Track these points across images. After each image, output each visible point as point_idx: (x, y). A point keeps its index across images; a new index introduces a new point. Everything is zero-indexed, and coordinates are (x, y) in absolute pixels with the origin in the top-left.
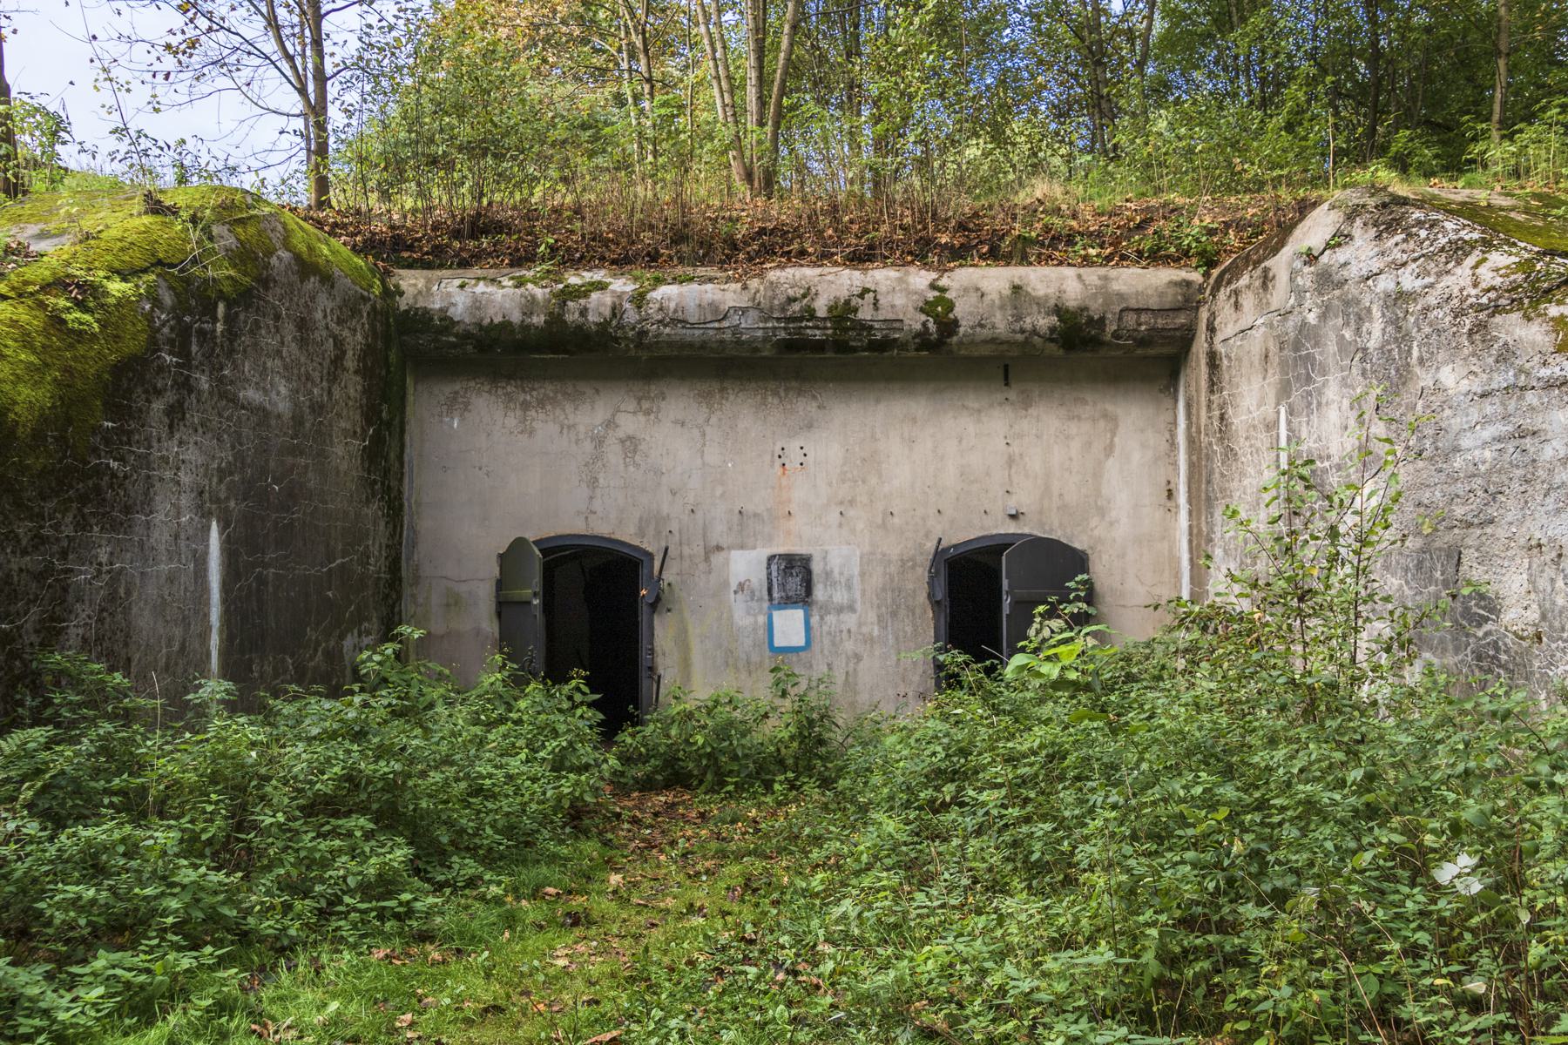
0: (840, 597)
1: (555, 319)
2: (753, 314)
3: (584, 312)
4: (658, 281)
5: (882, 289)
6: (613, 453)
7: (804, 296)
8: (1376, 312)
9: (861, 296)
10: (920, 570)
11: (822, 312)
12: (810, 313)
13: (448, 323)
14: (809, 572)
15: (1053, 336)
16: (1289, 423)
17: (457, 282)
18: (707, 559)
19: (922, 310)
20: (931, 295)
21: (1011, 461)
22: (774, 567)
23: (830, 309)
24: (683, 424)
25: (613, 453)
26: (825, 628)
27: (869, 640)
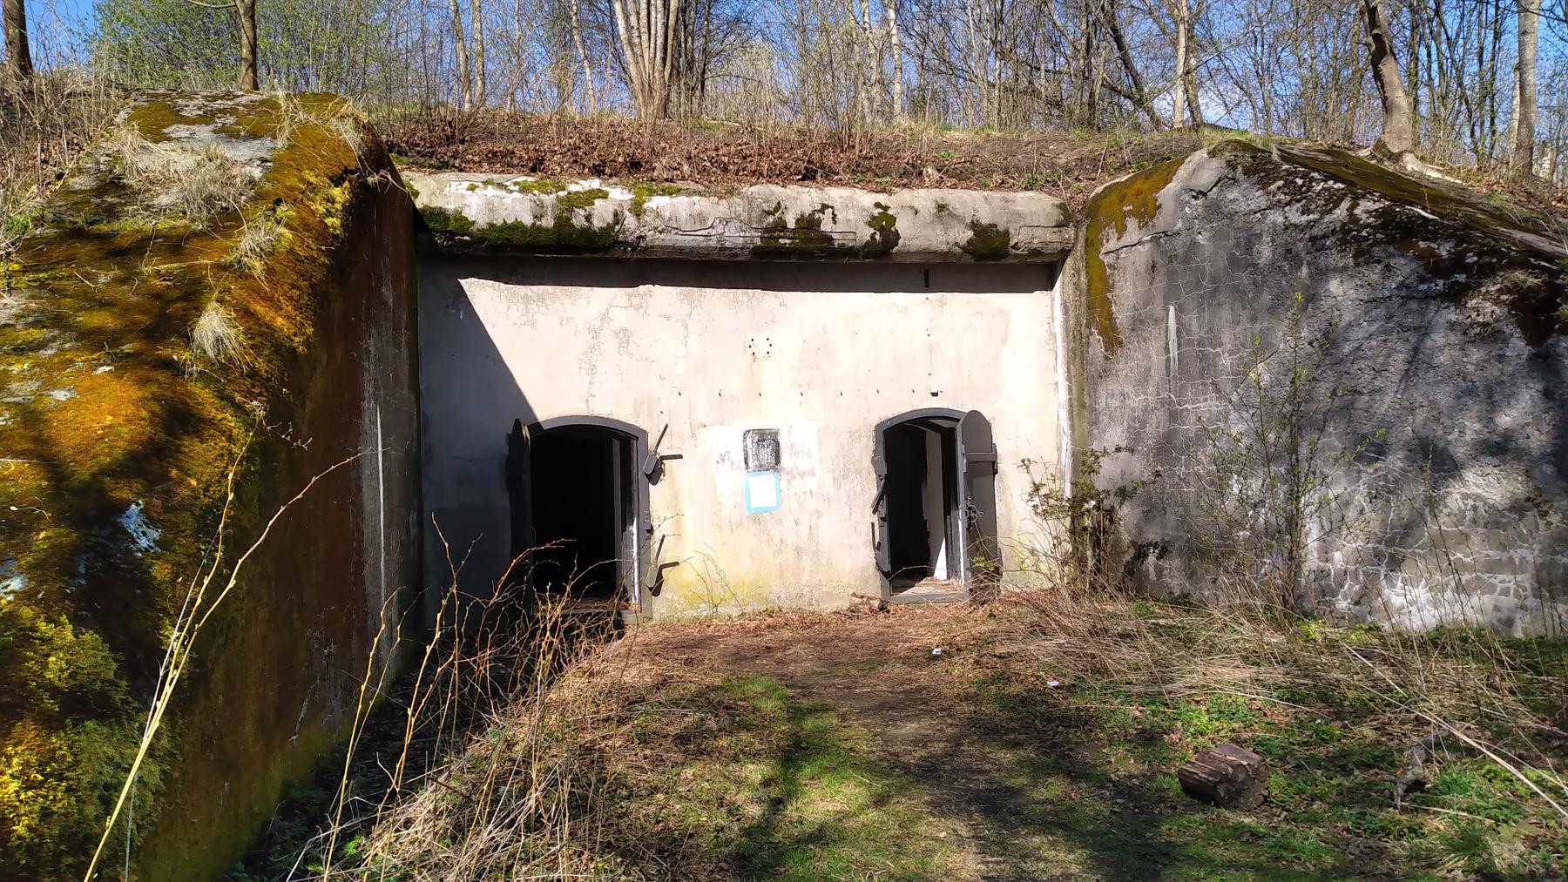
0: (803, 464)
1: (563, 223)
2: (734, 224)
3: (588, 218)
4: (652, 192)
5: (837, 205)
6: (609, 343)
8: (1266, 239)
9: (822, 211)
10: (864, 440)
11: (791, 225)
12: (781, 226)
13: (463, 223)
14: (778, 444)
15: (969, 249)
16: (1178, 318)
17: (466, 184)
18: (693, 435)
19: (870, 224)
20: (877, 212)
21: (931, 349)
22: (749, 441)
23: (798, 222)
24: (668, 318)
25: (609, 343)
26: (792, 490)
27: (827, 499)
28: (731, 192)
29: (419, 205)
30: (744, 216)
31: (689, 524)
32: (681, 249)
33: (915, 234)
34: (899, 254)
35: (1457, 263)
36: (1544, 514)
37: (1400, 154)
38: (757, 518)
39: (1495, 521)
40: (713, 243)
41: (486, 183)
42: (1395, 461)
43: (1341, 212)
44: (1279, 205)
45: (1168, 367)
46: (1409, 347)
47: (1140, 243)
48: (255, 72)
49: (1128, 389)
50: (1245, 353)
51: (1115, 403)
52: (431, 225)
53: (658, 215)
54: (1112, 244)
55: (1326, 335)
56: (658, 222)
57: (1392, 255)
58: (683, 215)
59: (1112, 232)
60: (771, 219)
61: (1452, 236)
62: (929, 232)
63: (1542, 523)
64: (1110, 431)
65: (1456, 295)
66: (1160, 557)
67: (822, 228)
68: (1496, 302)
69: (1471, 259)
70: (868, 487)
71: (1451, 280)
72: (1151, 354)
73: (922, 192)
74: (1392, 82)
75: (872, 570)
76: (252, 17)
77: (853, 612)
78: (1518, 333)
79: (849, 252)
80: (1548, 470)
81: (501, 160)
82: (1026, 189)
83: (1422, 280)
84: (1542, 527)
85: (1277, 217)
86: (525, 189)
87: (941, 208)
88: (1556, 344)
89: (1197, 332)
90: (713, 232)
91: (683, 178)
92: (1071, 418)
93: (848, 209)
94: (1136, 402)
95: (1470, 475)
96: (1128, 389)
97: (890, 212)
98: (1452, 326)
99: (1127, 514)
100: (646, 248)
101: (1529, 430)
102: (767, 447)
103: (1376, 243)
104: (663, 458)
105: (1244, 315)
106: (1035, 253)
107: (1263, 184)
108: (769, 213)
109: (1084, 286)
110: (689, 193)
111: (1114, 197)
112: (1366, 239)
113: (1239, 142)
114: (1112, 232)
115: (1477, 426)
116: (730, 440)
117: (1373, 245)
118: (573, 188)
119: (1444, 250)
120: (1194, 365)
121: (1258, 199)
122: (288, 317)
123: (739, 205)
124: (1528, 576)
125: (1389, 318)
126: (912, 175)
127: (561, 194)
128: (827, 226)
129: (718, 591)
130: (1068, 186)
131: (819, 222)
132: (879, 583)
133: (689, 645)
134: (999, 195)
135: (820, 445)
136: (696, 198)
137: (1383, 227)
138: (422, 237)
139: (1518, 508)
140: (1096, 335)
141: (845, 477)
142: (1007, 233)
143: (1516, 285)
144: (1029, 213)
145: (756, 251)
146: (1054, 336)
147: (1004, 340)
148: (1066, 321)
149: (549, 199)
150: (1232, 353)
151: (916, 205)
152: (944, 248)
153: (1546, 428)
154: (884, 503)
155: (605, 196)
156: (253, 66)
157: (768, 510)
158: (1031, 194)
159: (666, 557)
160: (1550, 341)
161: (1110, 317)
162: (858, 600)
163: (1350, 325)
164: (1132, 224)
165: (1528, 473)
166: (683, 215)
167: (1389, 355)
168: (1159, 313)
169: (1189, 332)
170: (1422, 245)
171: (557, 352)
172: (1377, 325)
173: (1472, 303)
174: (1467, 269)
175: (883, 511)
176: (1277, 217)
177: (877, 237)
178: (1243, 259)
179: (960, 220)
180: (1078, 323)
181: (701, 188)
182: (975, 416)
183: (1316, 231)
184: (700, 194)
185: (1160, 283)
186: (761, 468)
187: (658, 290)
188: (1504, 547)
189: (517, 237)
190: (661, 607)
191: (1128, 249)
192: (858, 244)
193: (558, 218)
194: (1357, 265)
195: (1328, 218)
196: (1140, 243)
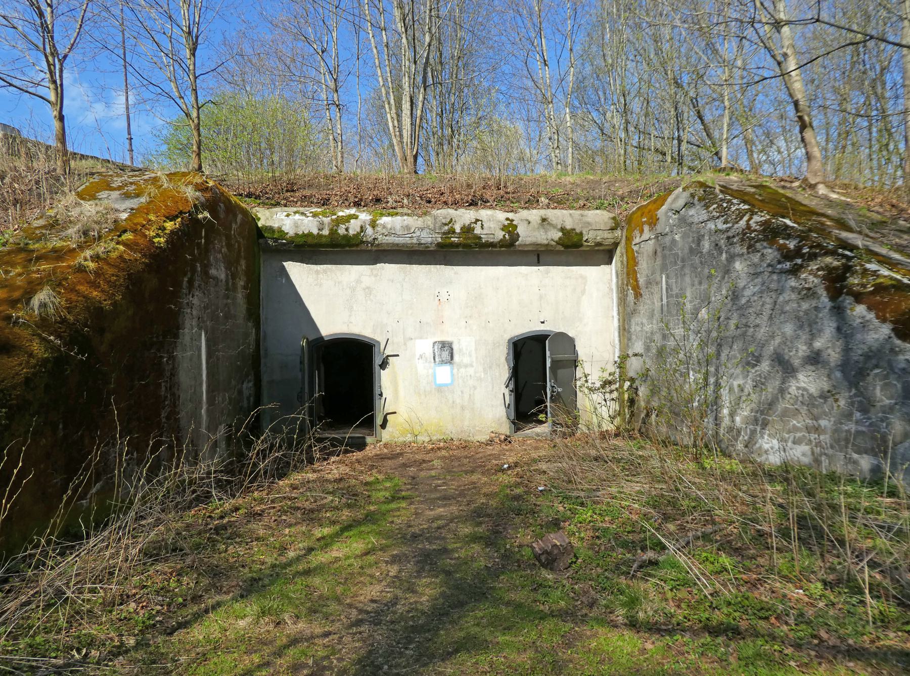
0: (466, 360)
1: (333, 232)
3: (347, 230)
4: (382, 215)
5: (484, 219)
7: (450, 223)
8: (707, 238)
10: (501, 347)
11: (458, 230)
14: (452, 349)
16: (667, 282)
17: (285, 214)
18: (405, 344)
19: (502, 230)
20: (506, 223)
21: (541, 297)
22: (436, 347)
23: (461, 229)
27: (480, 379)
28: (425, 214)
29: (260, 225)
30: (432, 226)
31: (402, 393)
32: (397, 245)
33: (528, 235)
34: (520, 245)
35: (798, 253)
36: (836, 400)
37: (816, 184)
38: (440, 389)
39: (810, 402)
40: (415, 241)
41: (295, 213)
42: (765, 366)
43: (743, 223)
44: (713, 218)
45: (662, 309)
46: (772, 300)
47: (649, 239)
48: (199, 157)
49: (645, 321)
50: (697, 302)
51: (638, 328)
52: (266, 235)
53: (384, 227)
54: (637, 240)
55: (734, 292)
56: (384, 231)
57: (765, 248)
58: (398, 227)
59: (637, 233)
60: (446, 228)
61: (798, 236)
62: (536, 233)
63: (835, 405)
64: (636, 344)
65: (795, 271)
66: (657, 416)
67: (475, 232)
68: (816, 276)
69: (806, 250)
70: (503, 372)
71: (793, 261)
72: (655, 300)
73: (535, 211)
74: (810, 143)
75: (504, 419)
76: (198, 129)
77: (490, 442)
78: (825, 293)
79: (492, 245)
80: (838, 374)
81: (307, 200)
82: (597, 209)
83: (779, 262)
84: (835, 408)
85: (711, 225)
86: (315, 215)
87: (544, 220)
88: (843, 301)
89: (676, 291)
90: (414, 235)
91: (402, 207)
92: (620, 336)
93: (490, 222)
94: (648, 328)
95: (801, 376)
96: (645, 321)
97: (514, 223)
98: (793, 289)
99: (643, 391)
100: (378, 245)
101: (830, 351)
102: (446, 351)
103: (759, 241)
104: (388, 356)
105: (696, 281)
106: (599, 244)
107: (707, 207)
108: (446, 224)
109: (625, 263)
110: (402, 215)
111: (639, 213)
112: (753, 238)
113: (699, 182)
114: (637, 233)
115: (804, 348)
116: (425, 347)
117: (756, 242)
118: (341, 214)
119: (792, 244)
120: (674, 305)
121: (704, 215)
122: (103, 291)
123: (429, 220)
124: (827, 436)
125: (763, 284)
126: (532, 202)
127: (334, 217)
128: (478, 231)
129: (417, 428)
130: (620, 206)
131: (473, 229)
132: (508, 426)
133: (394, 454)
134: (579, 212)
135: (476, 349)
136: (405, 217)
137: (764, 231)
138: (261, 241)
139: (824, 396)
140: (631, 288)
141: (490, 367)
142: (581, 234)
143: (827, 266)
144: (594, 222)
145: (439, 245)
146: (612, 290)
147: (583, 292)
148: (617, 282)
149: (327, 220)
150: (691, 302)
151: (530, 219)
152: (546, 242)
153: (838, 350)
154: (512, 382)
155: (356, 217)
156: (199, 155)
157: (446, 385)
158: (598, 211)
159: (388, 409)
160: (841, 299)
161: (636, 280)
162: (493, 435)
163: (744, 288)
164: (646, 228)
165: (829, 376)
166: (398, 227)
167: (763, 305)
168: (658, 279)
169: (671, 290)
170: (781, 242)
171: (334, 300)
172: (757, 288)
173: (803, 276)
174: (802, 256)
175: (512, 386)
176: (711, 225)
177: (507, 236)
178: (696, 250)
179: (554, 227)
180: (623, 284)
181: (410, 212)
182: (562, 336)
183: (730, 234)
184: (408, 215)
185: (659, 261)
186: (443, 362)
187: (383, 264)
188: (816, 418)
189: (310, 240)
190: (386, 435)
191: (645, 242)
192: (496, 240)
193: (331, 230)
194: (748, 253)
195: (736, 226)
196: (649, 239)
